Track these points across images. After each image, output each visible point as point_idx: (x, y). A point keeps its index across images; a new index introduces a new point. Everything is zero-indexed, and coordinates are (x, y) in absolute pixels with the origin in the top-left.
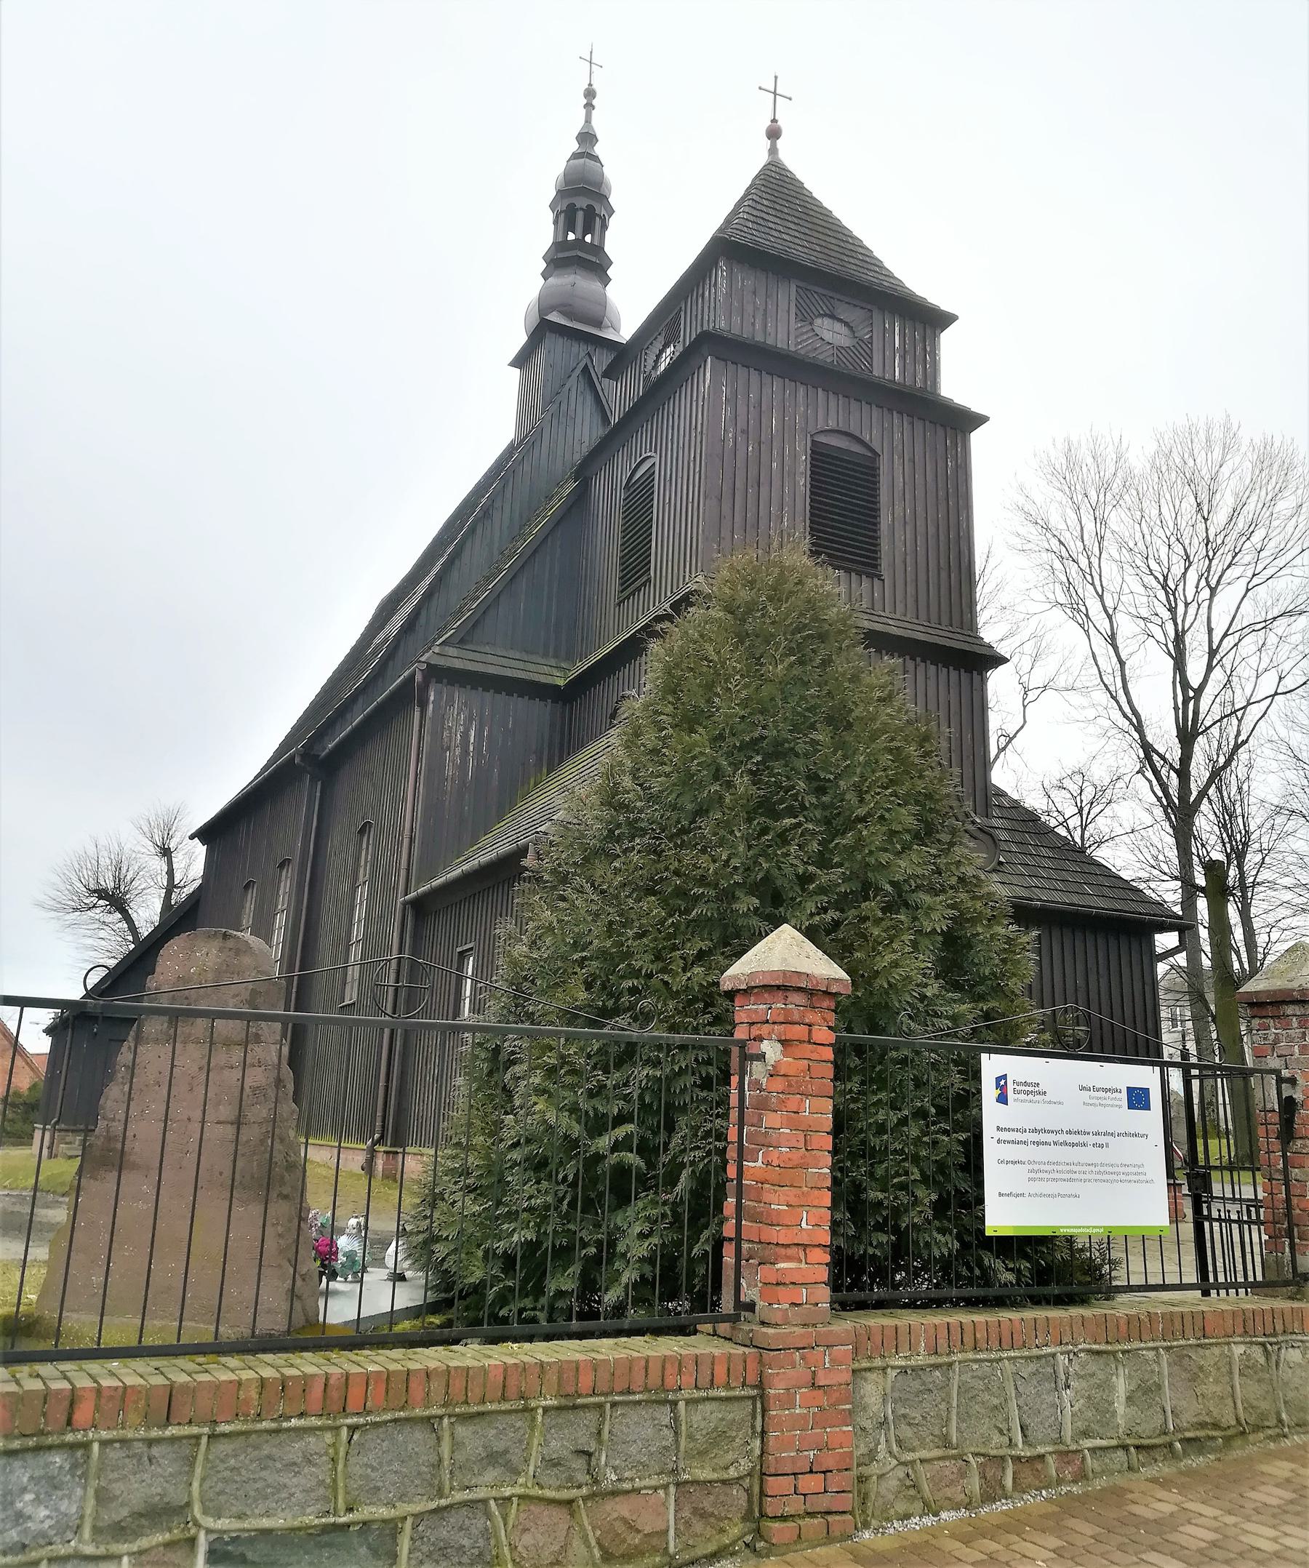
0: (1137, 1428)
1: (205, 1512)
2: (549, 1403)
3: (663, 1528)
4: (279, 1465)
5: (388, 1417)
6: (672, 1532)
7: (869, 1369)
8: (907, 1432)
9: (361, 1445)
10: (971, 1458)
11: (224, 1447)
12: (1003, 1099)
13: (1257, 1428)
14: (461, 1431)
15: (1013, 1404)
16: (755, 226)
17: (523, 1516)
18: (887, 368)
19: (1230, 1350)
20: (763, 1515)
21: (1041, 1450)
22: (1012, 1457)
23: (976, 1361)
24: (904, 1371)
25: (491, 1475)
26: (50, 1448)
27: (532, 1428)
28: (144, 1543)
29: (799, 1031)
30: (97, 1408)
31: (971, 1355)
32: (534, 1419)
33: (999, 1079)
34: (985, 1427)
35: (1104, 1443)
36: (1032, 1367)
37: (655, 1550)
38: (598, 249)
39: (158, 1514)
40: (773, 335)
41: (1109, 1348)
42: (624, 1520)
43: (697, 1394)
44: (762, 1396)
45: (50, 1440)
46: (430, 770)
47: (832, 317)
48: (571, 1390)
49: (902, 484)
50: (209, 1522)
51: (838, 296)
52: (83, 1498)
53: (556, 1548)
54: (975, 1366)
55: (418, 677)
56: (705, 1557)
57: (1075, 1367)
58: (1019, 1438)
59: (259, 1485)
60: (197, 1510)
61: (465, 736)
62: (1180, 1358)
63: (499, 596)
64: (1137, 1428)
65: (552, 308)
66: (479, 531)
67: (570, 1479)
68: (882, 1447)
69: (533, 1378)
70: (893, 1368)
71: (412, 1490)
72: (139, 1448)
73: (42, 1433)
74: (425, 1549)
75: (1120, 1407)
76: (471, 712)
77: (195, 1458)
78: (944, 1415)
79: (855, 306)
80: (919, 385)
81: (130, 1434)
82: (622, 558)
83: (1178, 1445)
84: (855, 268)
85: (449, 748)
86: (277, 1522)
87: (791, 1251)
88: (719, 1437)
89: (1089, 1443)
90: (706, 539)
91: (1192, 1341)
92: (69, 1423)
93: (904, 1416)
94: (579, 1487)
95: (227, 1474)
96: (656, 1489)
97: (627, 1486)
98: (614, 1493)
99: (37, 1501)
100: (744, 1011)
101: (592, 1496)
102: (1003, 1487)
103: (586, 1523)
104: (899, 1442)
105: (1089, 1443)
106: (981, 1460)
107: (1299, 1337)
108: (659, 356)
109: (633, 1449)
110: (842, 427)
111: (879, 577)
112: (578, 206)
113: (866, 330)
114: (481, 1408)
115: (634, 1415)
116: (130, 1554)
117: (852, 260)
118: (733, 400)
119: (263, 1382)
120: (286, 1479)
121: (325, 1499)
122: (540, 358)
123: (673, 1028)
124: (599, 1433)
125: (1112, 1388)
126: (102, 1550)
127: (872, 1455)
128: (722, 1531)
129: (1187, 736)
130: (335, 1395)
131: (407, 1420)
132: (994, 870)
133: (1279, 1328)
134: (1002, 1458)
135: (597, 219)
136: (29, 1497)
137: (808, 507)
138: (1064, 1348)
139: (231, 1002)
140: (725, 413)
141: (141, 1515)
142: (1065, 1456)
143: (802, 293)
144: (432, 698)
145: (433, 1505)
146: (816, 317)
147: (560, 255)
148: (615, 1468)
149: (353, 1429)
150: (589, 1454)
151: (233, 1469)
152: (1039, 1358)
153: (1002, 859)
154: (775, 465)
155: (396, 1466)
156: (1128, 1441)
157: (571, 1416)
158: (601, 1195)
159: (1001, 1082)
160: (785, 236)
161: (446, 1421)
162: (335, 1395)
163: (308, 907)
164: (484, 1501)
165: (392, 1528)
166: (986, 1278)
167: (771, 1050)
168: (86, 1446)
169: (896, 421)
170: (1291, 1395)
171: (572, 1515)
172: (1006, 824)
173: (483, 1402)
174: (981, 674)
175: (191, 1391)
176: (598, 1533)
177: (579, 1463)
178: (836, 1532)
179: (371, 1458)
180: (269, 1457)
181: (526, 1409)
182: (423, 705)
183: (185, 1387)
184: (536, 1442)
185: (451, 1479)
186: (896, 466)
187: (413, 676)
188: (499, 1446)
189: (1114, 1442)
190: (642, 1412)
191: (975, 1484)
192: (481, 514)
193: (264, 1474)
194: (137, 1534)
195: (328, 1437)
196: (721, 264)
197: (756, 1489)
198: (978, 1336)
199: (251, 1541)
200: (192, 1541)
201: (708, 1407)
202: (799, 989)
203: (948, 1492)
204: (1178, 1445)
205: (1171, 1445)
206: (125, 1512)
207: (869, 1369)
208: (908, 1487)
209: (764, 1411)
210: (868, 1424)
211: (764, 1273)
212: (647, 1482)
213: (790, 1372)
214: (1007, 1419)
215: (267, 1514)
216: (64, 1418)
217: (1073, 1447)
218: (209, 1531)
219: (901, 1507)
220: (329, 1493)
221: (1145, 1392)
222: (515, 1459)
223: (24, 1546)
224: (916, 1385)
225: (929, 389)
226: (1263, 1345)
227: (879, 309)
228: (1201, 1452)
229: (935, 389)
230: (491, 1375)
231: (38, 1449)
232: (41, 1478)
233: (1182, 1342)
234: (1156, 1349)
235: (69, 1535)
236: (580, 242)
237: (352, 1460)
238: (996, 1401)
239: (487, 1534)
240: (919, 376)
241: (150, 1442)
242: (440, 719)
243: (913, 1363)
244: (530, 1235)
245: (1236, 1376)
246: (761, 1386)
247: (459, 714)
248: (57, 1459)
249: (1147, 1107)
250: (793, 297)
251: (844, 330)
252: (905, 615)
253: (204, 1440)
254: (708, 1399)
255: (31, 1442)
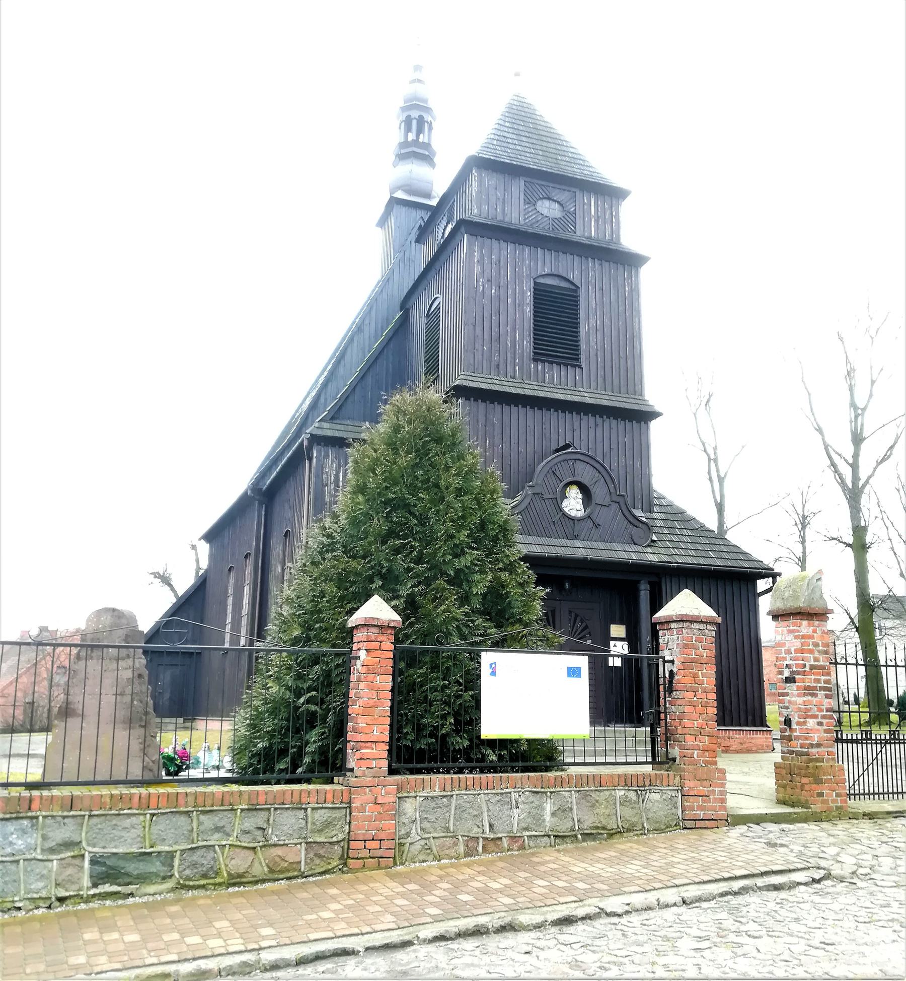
0: (557, 828)
1: (89, 845)
2: (244, 807)
3: (299, 860)
4: (120, 828)
5: (168, 810)
6: (303, 863)
7: (408, 797)
8: (426, 825)
9: (155, 821)
10: (460, 837)
11: (95, 820)
12: (493, 673)
13: (629, 830)
14: (202, 817)
15: (485, 814)
16: (499, 143)
17: (231, 853)
18: (586, 229)
19: (615, 793)
20: (348, 857)
21: (500, 835)
22: (483, 838)
23: (466, 794)
24: (426, 798)
25: (217, 836)
26: (22, 818)
27: (236, 817)
28: (62, 856)
29: (375, 645)
30: (41, 803)
31: (463, 792)
32: (236, 814)
33: (491, 665)
34: (470, 824)
35: (536, 834)
36: (498, 798)
37: (295, 870)
38: (427, 146)
39: (68, 845)
40: (509, 215)
41: (543, 790)
42: (279, 856)
43: (316, 805)
44: (350, 807)
45: (21, 815)
46: (316, 499)
47: (549, 199)
48: (255, 802)
49: (594, 305)
50: (90, 849)
51: (551, 184)
52: (37, 838)
53: (247, 866)
54: (465, 797)
55: (305, 443)
56: (319, 873)
57: (523, 798)
58: (487, 829)
59: (111, 836)
60: (84, 844)
61: (337, 476)
62: (585, 796)
63: (354, 388)
64: (557, 828)
65: (399, 188)
66: (356, 339)
67: (254, 839)
68: (413, 831)
69: (236, 796)
70: (420, 796)
71: (180, 841)
72: (59, 819)
73: (18, 812)
74: (186, 864)
75: (547, 817)
76: (340, 463)
77: (83, 824)
78: (447, 818)
79: (564, 190)
80: (607, 238)
81: (55, 814)
82: (425, 361)
83: (579, 836)
84: (565, 163)
85: (327, 485)
86: (120, 850)
87: (367, 745)
88: (328, 825)
89: (528, 833)
90: (466, 351)
91: (593, 788)
92: (30, 809)
93: (426, 818)
94: (259, 842)
95: (97, 831)
96: (296, 844)
97: (282, 843)
98: (275, 845)
99: (18, 838)
100: (359, 636)
101: (264, 846)
102: (478, 851)
103: (261, 857)
104: (423, 829)
105: (528, 833)
106: (466, 838)
107: (659, 788)
108: (444, 230)
109: (285, 828)
110: (554, 271)
111: (580, 367)
112: (413, 117)
113: (572, 206)
114: (212, 808)
115: (286, 814)
116: (57, 860)
117: (564, 158)
118: (481, 261)
119: (112, 795)
120: (123, 834)
121: (141, 843)
122: (392, 220)
123: (334, 646)
124: (268, 820)
125: (543, 809)
126: (45, 858)
127: (408, 835)
128: (329, 863)
129: (857, 439)
130: (144, 801)
131: (177, 812)
132: (649, 546)
133: (647, 783)
134: (478, 838)
135: (426, 124)
136: (14, 836)
137: (532, 325)
138: (516, 790)
139: (117, 640)
140: (477, 269)
141: (61, 845)
142: (513, 838)
143: (528, 185)
144: (315, 455)
145: (189, 847)
146: (538, 200)
147: (403, 151)
148: (277, 836)
149: (153, 815)
150: (264, 829)
151: (100, 829)
152: (502, 794)
153: (654, 538)
154: (509, 300)
155: (173, 831)
156: (550, 833)
157: (255, 813)
158: (302, 725)
159: (493, 667)
160: (518, 148)
161: (195, 813)
162: (144, 801)
163: (261, 582)
164: (213, 846)
165: (171, 855)
166: (483, 758)
167: (363, 654)
168: (37, 818)
169: (590, 264)
170: (650, 815)
171: (255, 853)
172: (663, 516)
173: (212, 806)
174: (646, 423)
175: (81, 798)
176: (267, 861)
177: (260, 833)
178: (383, 864)
179: (161, 827)
180: (115, 825)
181: (232, 810)
182: (310, 459)
183: (78, 796)
184: (237, 823)
185: (198, 837)
186: (590, 294)
187: (302, 442)
188: (220, 824)
189: (542, 834)
190: (290, 812)
191: (461, 849)
192: (356, 330)
193: (114, 831)
194: (59, 853)
195: (142, 818)
196: (474, 172)
197: (346, 847)
198: (468, 783)
199: (108, 857)
200: (83, 856)
201: (323, 811)
202: (375, 626)
203: (447, 852)
204: (579, 836)
205: (576, 836)
206: (54, 844)
207: (408, 797)
208: (427, 849)
209: (350, 813)
210: (406, 821)
211: (358, 755)
212: (291, 841)
213: (363, 797)
214: (482, 821)
215: (115, 847)
216: (27, 807)
217: (518, 835)
218: (90, 852)
219: (421, 857)
220: (142, 840)
221: (562, 811)
222: (228, 829)
223: (13, 854)
224: (433, 805)
225: (614, 240)
226: (636, 791)
227: (580, 190)
228: (594, 840)
229: (619, 240)
230: (216, 796)
231: (17, 818)
232: (19, 829)
233: (586, 789)
234: (571, 791)
235: (32, 851)
236: (416, 142)
237: (152, 828)
238: (476, 813)
239: (215, 859)
240: (608, 232)
241: (64, 817)
242: (321, 467)
243: (431, 795)
244: (266, 744)
245: (618, 805)
246: (350, 803)
247: (332, 464)
248: (25, 822)
249: (579, 676)
250: (522, 189)
251: (556, 206)
252: (597, 389)
253: (87, 817)
254: (322, 808)
255: (14, 815)
